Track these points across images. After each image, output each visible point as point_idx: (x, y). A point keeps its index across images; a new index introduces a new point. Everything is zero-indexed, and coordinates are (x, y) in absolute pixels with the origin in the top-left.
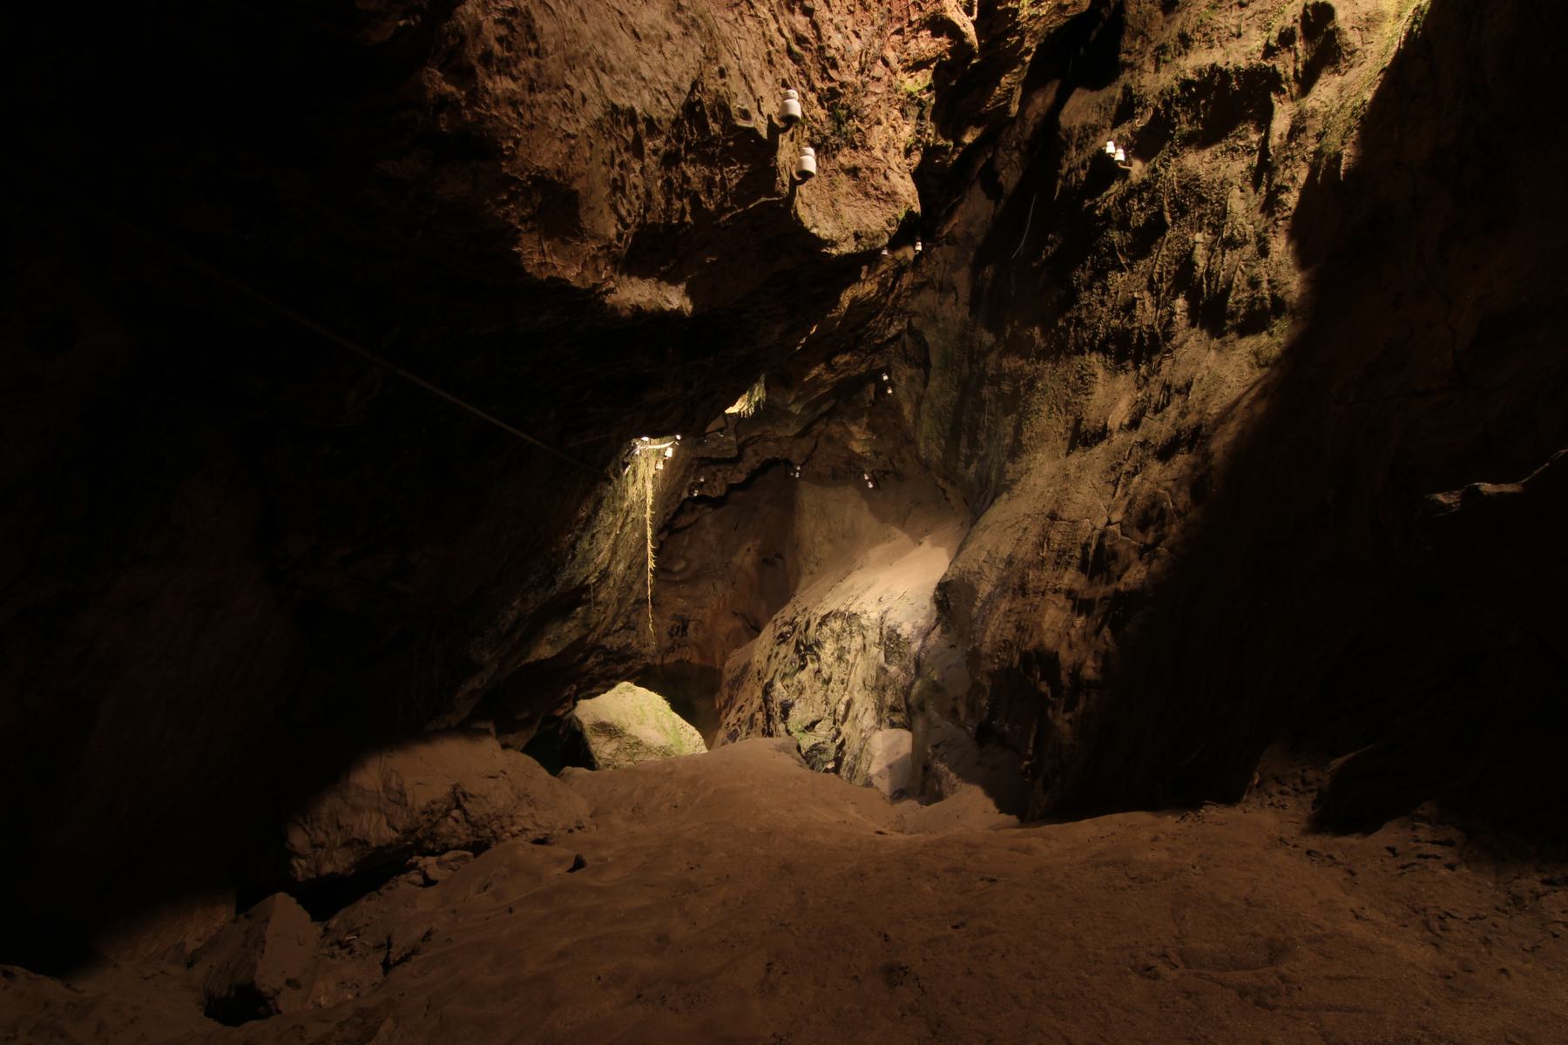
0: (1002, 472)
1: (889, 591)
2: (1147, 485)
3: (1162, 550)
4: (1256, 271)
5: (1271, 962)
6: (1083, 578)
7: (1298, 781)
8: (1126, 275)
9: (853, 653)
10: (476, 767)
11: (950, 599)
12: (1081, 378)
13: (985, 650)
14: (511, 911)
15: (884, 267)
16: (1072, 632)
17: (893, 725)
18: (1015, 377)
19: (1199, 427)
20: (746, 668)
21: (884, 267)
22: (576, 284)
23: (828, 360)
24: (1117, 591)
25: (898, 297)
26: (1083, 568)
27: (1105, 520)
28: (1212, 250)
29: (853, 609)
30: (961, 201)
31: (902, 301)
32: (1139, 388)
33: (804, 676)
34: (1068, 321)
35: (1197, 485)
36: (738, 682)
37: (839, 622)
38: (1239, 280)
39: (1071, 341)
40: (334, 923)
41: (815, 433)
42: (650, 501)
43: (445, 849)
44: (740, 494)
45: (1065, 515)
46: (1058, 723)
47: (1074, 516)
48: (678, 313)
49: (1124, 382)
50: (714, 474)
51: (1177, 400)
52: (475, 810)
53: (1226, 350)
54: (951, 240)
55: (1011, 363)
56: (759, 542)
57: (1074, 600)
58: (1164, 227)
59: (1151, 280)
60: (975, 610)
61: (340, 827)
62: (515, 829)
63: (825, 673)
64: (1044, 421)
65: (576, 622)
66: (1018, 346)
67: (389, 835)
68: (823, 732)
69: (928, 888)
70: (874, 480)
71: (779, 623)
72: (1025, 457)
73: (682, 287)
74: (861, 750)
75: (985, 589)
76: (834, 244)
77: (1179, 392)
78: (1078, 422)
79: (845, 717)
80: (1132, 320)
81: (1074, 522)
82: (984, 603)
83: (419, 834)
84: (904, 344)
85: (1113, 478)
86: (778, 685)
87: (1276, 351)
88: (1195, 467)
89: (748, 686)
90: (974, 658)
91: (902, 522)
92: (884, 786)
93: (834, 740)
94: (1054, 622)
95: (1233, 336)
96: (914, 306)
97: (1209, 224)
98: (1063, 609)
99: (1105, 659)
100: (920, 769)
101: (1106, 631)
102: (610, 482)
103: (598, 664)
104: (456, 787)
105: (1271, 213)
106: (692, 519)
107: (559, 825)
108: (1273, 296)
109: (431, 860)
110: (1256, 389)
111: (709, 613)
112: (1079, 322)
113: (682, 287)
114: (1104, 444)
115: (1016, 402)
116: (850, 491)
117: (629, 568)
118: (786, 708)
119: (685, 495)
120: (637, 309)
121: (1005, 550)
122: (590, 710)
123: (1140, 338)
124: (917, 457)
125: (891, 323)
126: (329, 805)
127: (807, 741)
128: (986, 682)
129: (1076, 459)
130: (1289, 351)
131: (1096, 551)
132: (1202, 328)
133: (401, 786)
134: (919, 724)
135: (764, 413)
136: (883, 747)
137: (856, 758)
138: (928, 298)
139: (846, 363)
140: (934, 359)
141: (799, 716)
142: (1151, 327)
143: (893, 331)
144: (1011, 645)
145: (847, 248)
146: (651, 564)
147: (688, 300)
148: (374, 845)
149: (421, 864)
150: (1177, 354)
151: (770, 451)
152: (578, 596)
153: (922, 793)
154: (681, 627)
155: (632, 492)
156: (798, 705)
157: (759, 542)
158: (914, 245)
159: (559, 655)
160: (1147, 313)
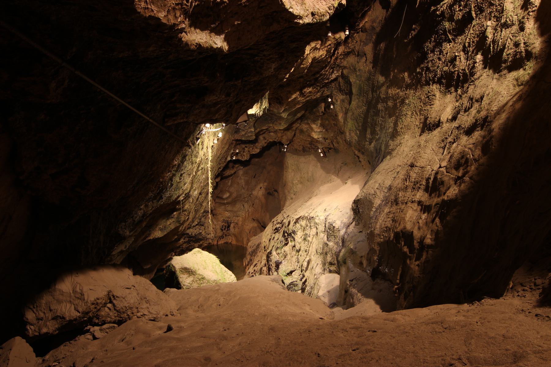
0: (387, 146)
1: (327, 206)
2: (460, 147)
3: (467, 179)
4: (518, 38)
5: (515, 362)
6: (427, 195)
7: (532, 284)
8: (452, 44)
9: (311, 237)
10: (119, 283)
11: (360, 208)
12: (428, 97)
13: (377, 232)
14: (134, 349)
15: (329, 42)
16: (420, 221)
17: (330, 272)
18: (395, 98)
19: (487, 117)
20: (258, 246)
21: (329, 42)
22: (164, 21)
23: (301, 90)
24: (443, 200)
25: (336, 59)
26: (426, 190)
27: (438, 166)
28: (496, 29)
29: (312, 215)
30: (369, 10)
31: (338, 61)
32: (457, 101)
33: (287, 249)
34: (422, 69)
35: (485, 146)
36: (254, 253)
37: (305, 222)
38: (510, 44)
39: (423, 79)
40: (47, 357)
41: (294, 128)
42: (210, 158)
43: (104, 323)
44: (257, 160)
45: (418, 165)
46: (412, 266)
47: (422, 165)
48: (220, 50)
49: (450, 98)
50: (244, 149)
51: (476, 105)
52: (120, 304)
53: (501, 79)
54: (364, 30)
55: (392, 91)
56: (266, 184)
57: (422, 206)
58: (471, 19)
59: (464, 46)
60: (372, 213)
61: (51, 310)
62: (139, 314)
63: (297, 248)
64: (409, 119)
65: (173, 220)
66: (396, 83)
67: (75, 314)
68: (296, 276)
69: (342, 335)
70: (324, 153)
71: (275, 223)
72: (399, 138)
73: (223, 36)
74: (315, 284)
75: (377, 202)
76: (301, 18)
77: (477, 101)
78: (426, 119)
79: (307, 269)
80: (454, 67)
81: (422, 167)
82: (377, 209)
83: (91, 314)
84: (339, 82)
85: (443, 145)
86: (274, 253)
87: (527, 78)
88: (484, 137)
89: (259, 254)
90: (371, 236)
91: (337, 173)
92: (326, 300)
93: (301, 280)
94: (412, 218)
95: (505, 72)
96: (345, 63)
97: (494, 16)
98: (416, 210)
99: (437, 234)
100: (343, 292)
101: (437, 220)
102: (190, 147)
103: (185, 243)
104: (109, 292)
105: (527, 9)
106: (233, 172)
107: (161, 313)
108: (526, 51)
109: (97, 328)
110: (516, 97)
111: (241, 219)
112: (428, 69)
113: (223, 36)
114: (439, 129)
115: (395, 111)
116: (312, 158)
117: (200, 194)
118: (278, 265)
119: (229, 159)
120: (199, 46)
121: (388, 183)
122: (179, 262)
123: (458, 76)
124: (345, 140)
125: (333, 72)
126: (46, 299)
127: (288, 280)
128: (377, 248)
129: (424, 137)
130: (534, 77)
131: (433, 181)
132: (489, 69)
133: (82, 290)
134: (343, 270)
135: (267, 116)
136: (326, 282)
137: (312, 288)
138: (352, 59)
139: (310, 92)
140: (354, 90)
141: (284, 268)
142: (464, 70)
143: (334, 76)
144: (390, 229)
145: (308, 20)
146: (211, 190)
147: (225, 44)
148: (67, 319)
149: (91, 330)
150: (477, 83)
151: (272, 137)
152: (174, 206)
153: (344, 304)
154: (227, 226)
155: (201, 153)
156: (284, 263)
157: (266, 184)
158: (345, 32)
159: (165, 236)
160: (462, 63)
